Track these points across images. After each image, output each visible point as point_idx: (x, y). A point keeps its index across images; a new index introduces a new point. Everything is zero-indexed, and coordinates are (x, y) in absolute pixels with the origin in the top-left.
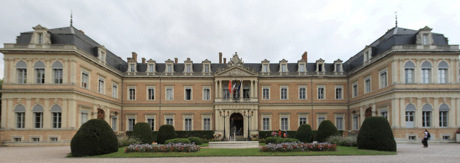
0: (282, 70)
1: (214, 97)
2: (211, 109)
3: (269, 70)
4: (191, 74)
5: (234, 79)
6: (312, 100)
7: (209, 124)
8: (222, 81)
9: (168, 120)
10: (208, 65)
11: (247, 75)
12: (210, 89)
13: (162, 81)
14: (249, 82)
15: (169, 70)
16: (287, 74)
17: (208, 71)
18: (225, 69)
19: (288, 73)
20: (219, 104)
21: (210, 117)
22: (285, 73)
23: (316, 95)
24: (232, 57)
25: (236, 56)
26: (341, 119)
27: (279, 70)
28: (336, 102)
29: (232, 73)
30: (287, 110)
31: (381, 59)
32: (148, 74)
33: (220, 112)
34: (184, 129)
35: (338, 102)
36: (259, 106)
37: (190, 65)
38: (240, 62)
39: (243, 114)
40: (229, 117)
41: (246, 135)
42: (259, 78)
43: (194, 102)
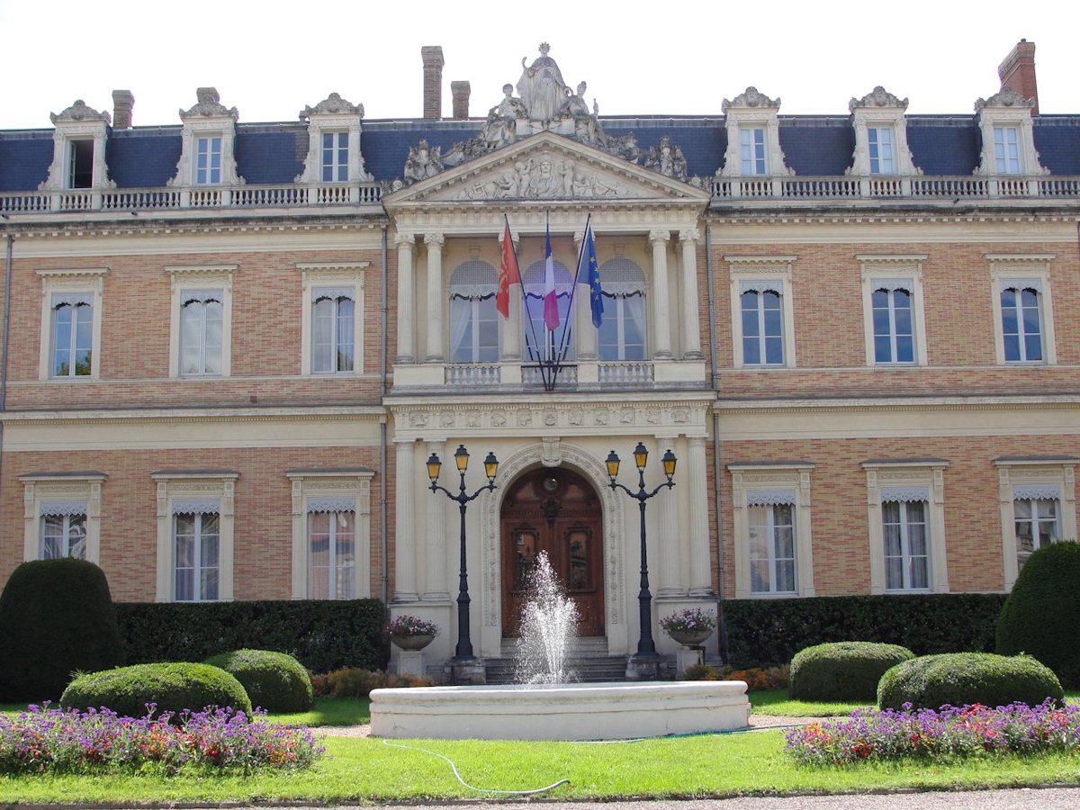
0: (875, 165)
8: (449, 239)
11: (624, 190)
12: (358, 297)
17: (343, 174)
18: (470, 155)
22: (895, 181)
24: (515, 75)
25: (545, 66)
34: (164, 593)
38: (571, 108)
39: (599, 478)
40: (499, 494)
42: (713, 213)
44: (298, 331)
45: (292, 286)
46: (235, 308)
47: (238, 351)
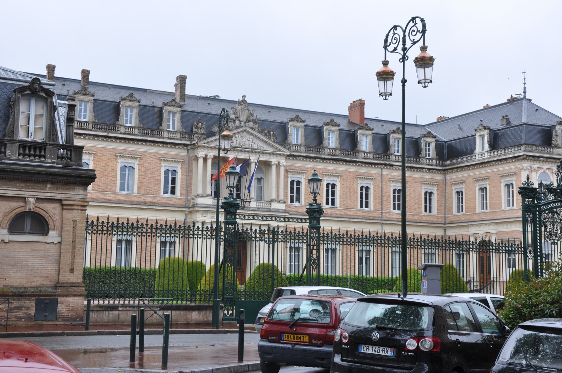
11: (266, 148)
23: (389, 203)
26: (298, 249)
28: (424, 219)
31: (506, 159)
35: (428, 219)
45: (158, 165)
46: (139, 170)
47: (140, 185)
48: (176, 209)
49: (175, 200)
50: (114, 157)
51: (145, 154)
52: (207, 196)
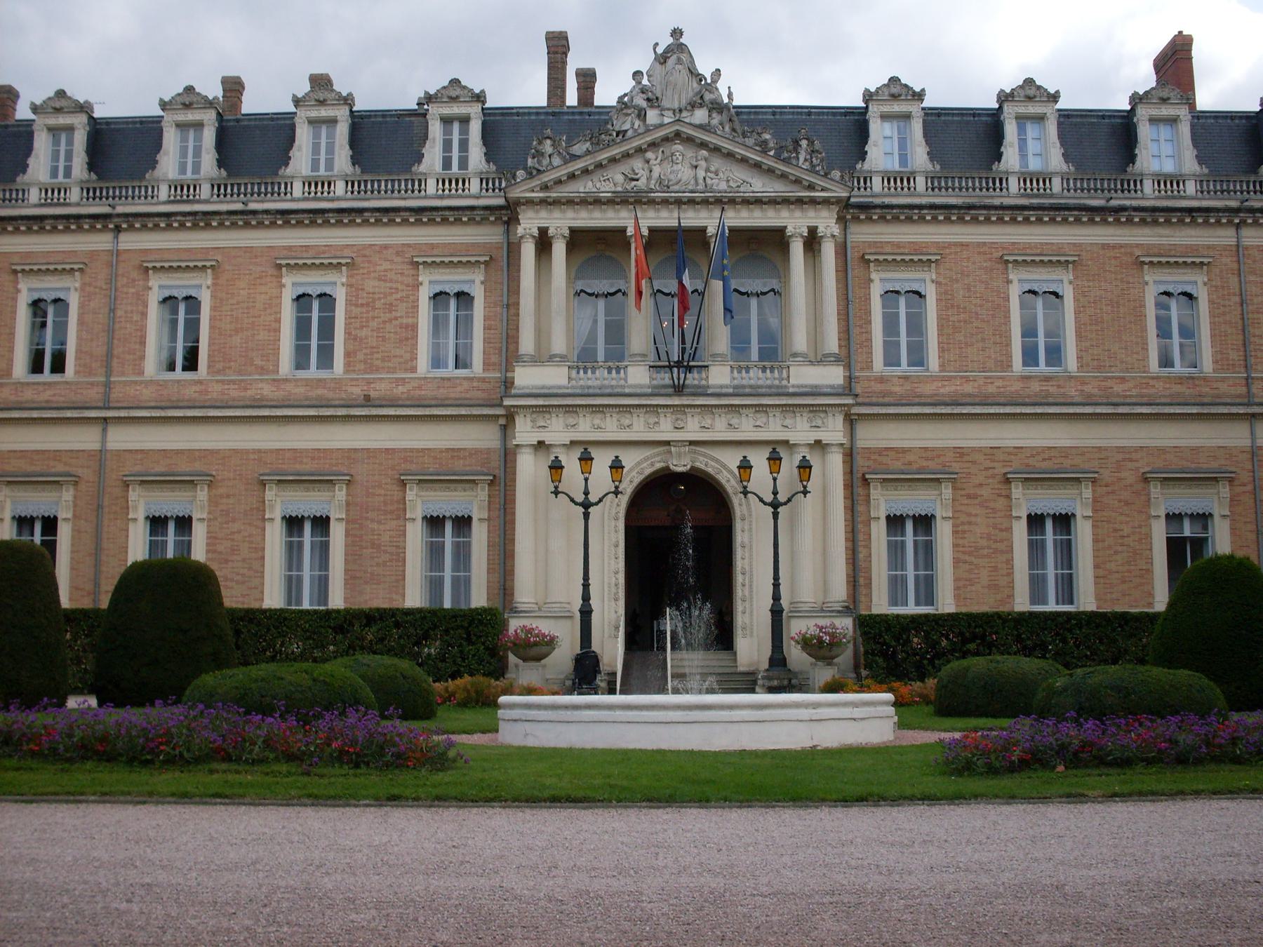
1: (506, 351)
2: (481, 437)
3: (920, 156)
4: (340, 188)
5: (666, 219)
6: (1248, 381)
7: (463, 556)
8: (573, 231)
9: (157, 524)
10: (465, 120)
11: (759, 185)
12: (478, 292)
13: (131, 241)
14: (777, 239)
15: (185, 160)
16: (1057, 185)
17: (463, 163)
18: (597, 144)
19: (1065, 178)
20: (548, 404)
21: (474, 503)
22: (1045, 178)
24: (645, 62)
25: (675, 52)
27: (998, 157)
29: (648, 172)
30: (1065, 452)
32: (34, 195)
33: (556, 467)
36: (851, 421)
37: (333, 122)
38: (704, 93)
39: (729, 483)
40: (624, 500)
41: (751, 646)
42: (850, 212)
43: (357, 391)
44: (414, 328)
45: (410, 280)
46: (348, 303)
48: (463, 411)
49: (466, 384)
50: (272, 271)
51: (367, 252)
52: (551, 358)
